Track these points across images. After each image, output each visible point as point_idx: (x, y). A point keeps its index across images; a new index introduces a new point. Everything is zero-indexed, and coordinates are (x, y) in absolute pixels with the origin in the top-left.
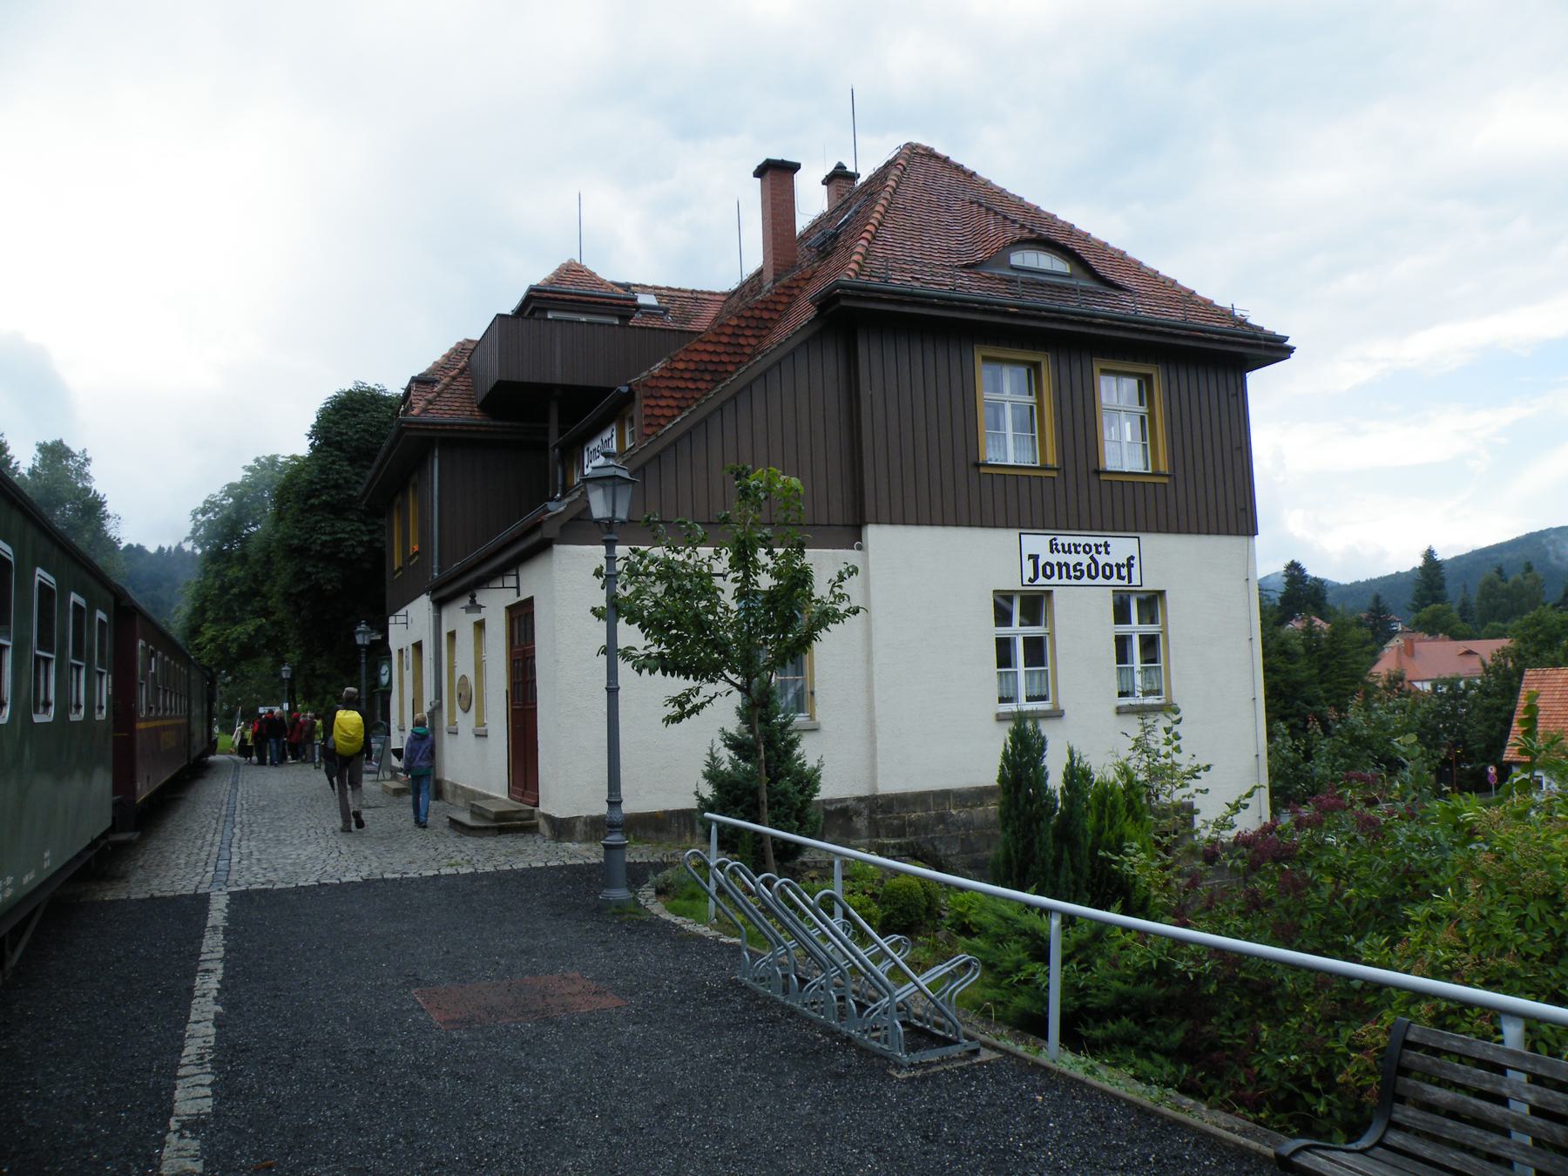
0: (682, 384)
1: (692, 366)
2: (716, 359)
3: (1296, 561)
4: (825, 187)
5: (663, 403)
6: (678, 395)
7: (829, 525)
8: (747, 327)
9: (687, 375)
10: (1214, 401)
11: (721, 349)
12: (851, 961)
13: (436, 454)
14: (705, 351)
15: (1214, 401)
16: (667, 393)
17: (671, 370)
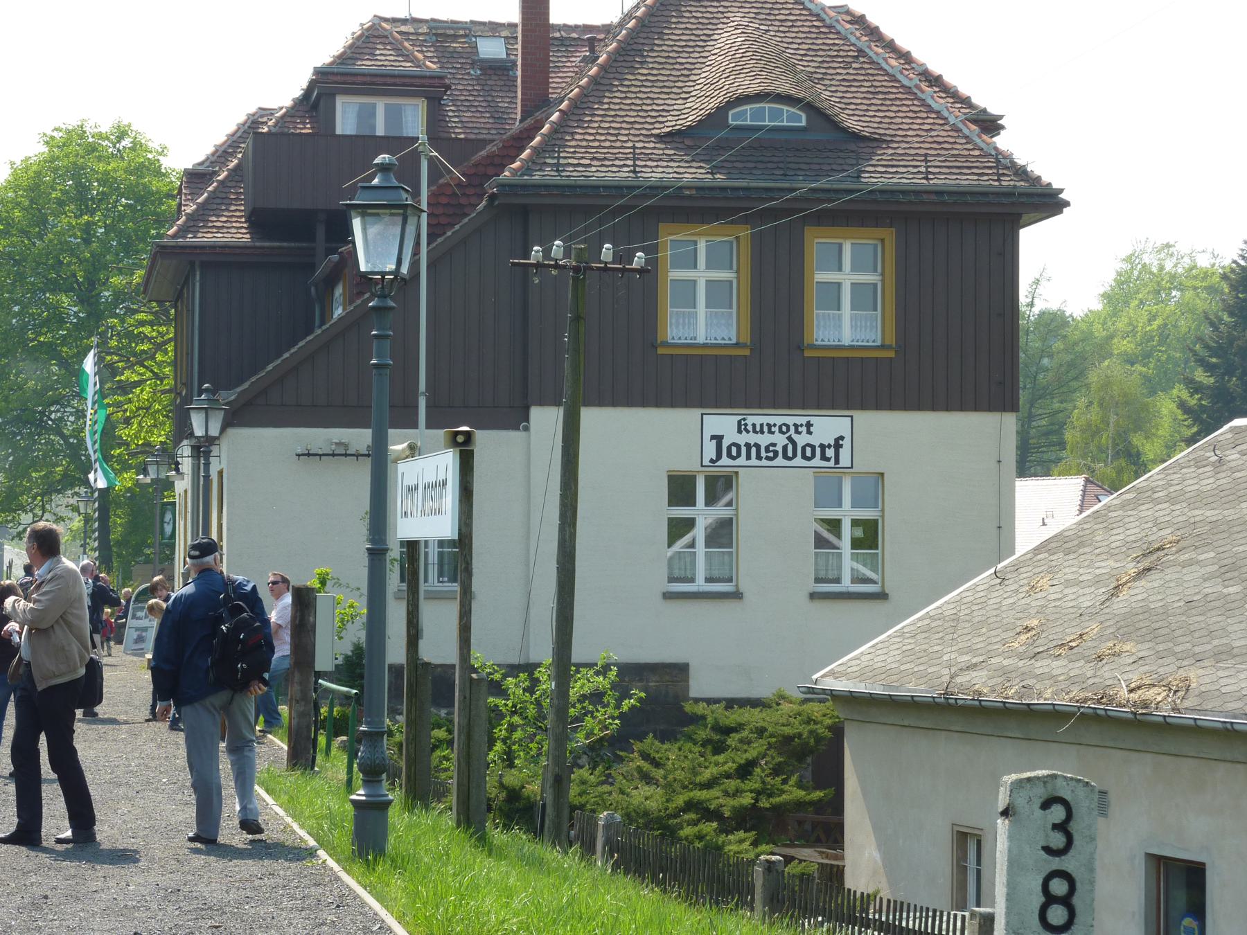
13: (198, 277)
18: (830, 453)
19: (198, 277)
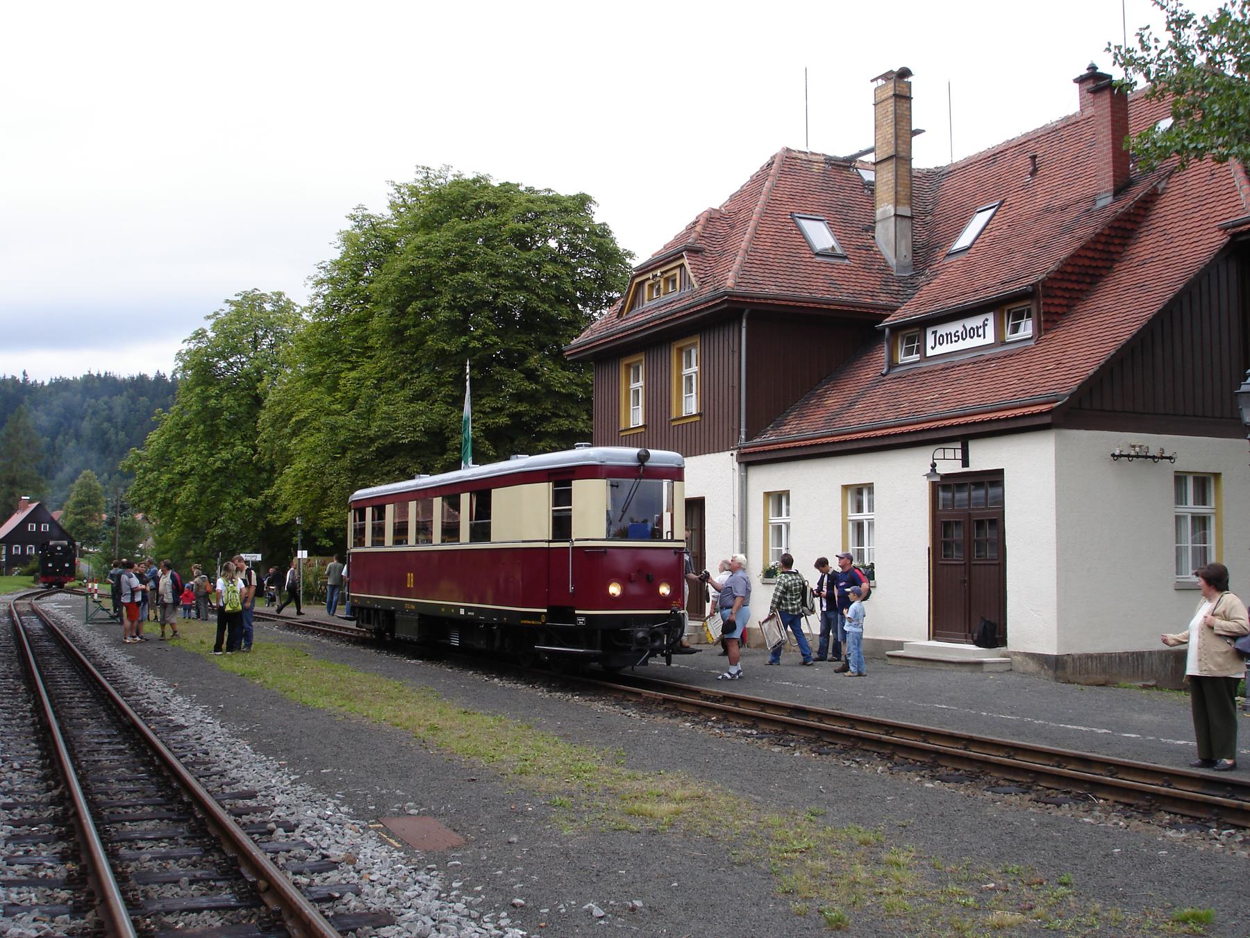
0: (1070, 286)
1: (1077, 270)
2: (1094, 264)
3: (162, 373)
4: (1077, 85)
5: (1056, 301)
6: (1067, 295)
7: (1165, 414)
8: (1116, 236)
9: (1074, 278)
10: (721, 353)
11: (1097, 256)
12: (986, 560)
13: (744, 324)
14: (1086, 256)
15: (721, 353)
16: (1059, 293)
17: (1062, 272)
18: (981, 332)
19: (744, 324)
